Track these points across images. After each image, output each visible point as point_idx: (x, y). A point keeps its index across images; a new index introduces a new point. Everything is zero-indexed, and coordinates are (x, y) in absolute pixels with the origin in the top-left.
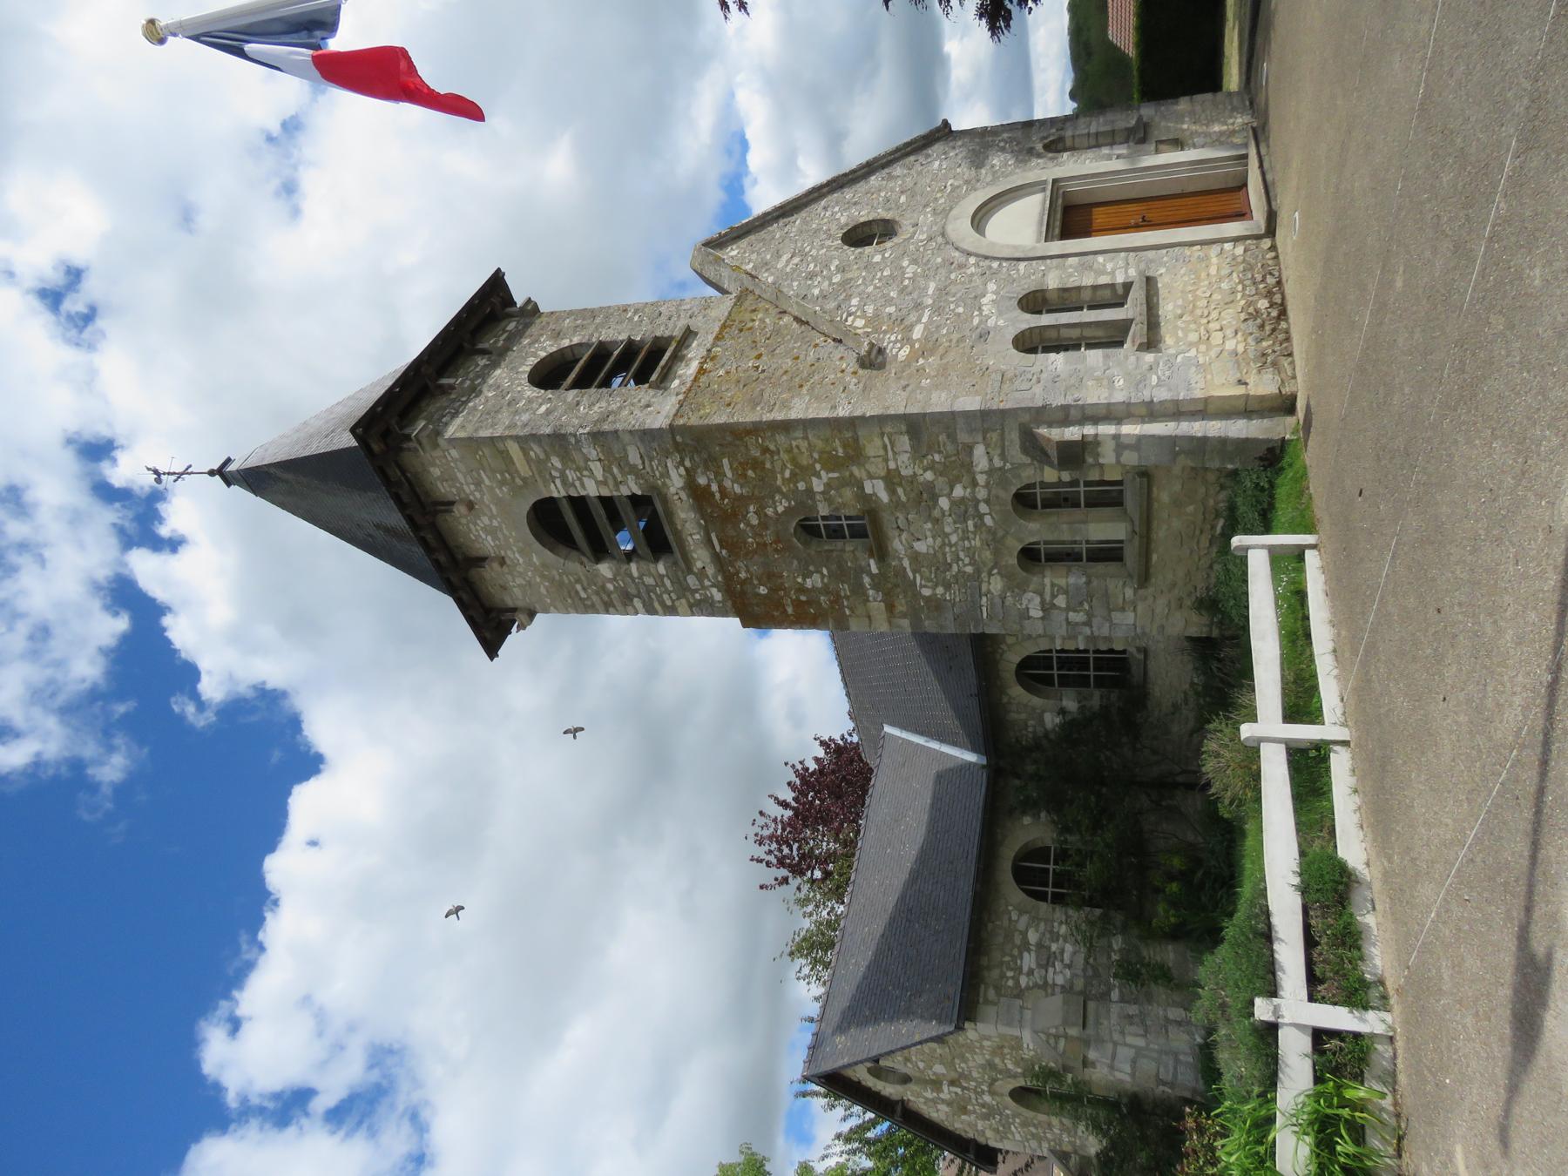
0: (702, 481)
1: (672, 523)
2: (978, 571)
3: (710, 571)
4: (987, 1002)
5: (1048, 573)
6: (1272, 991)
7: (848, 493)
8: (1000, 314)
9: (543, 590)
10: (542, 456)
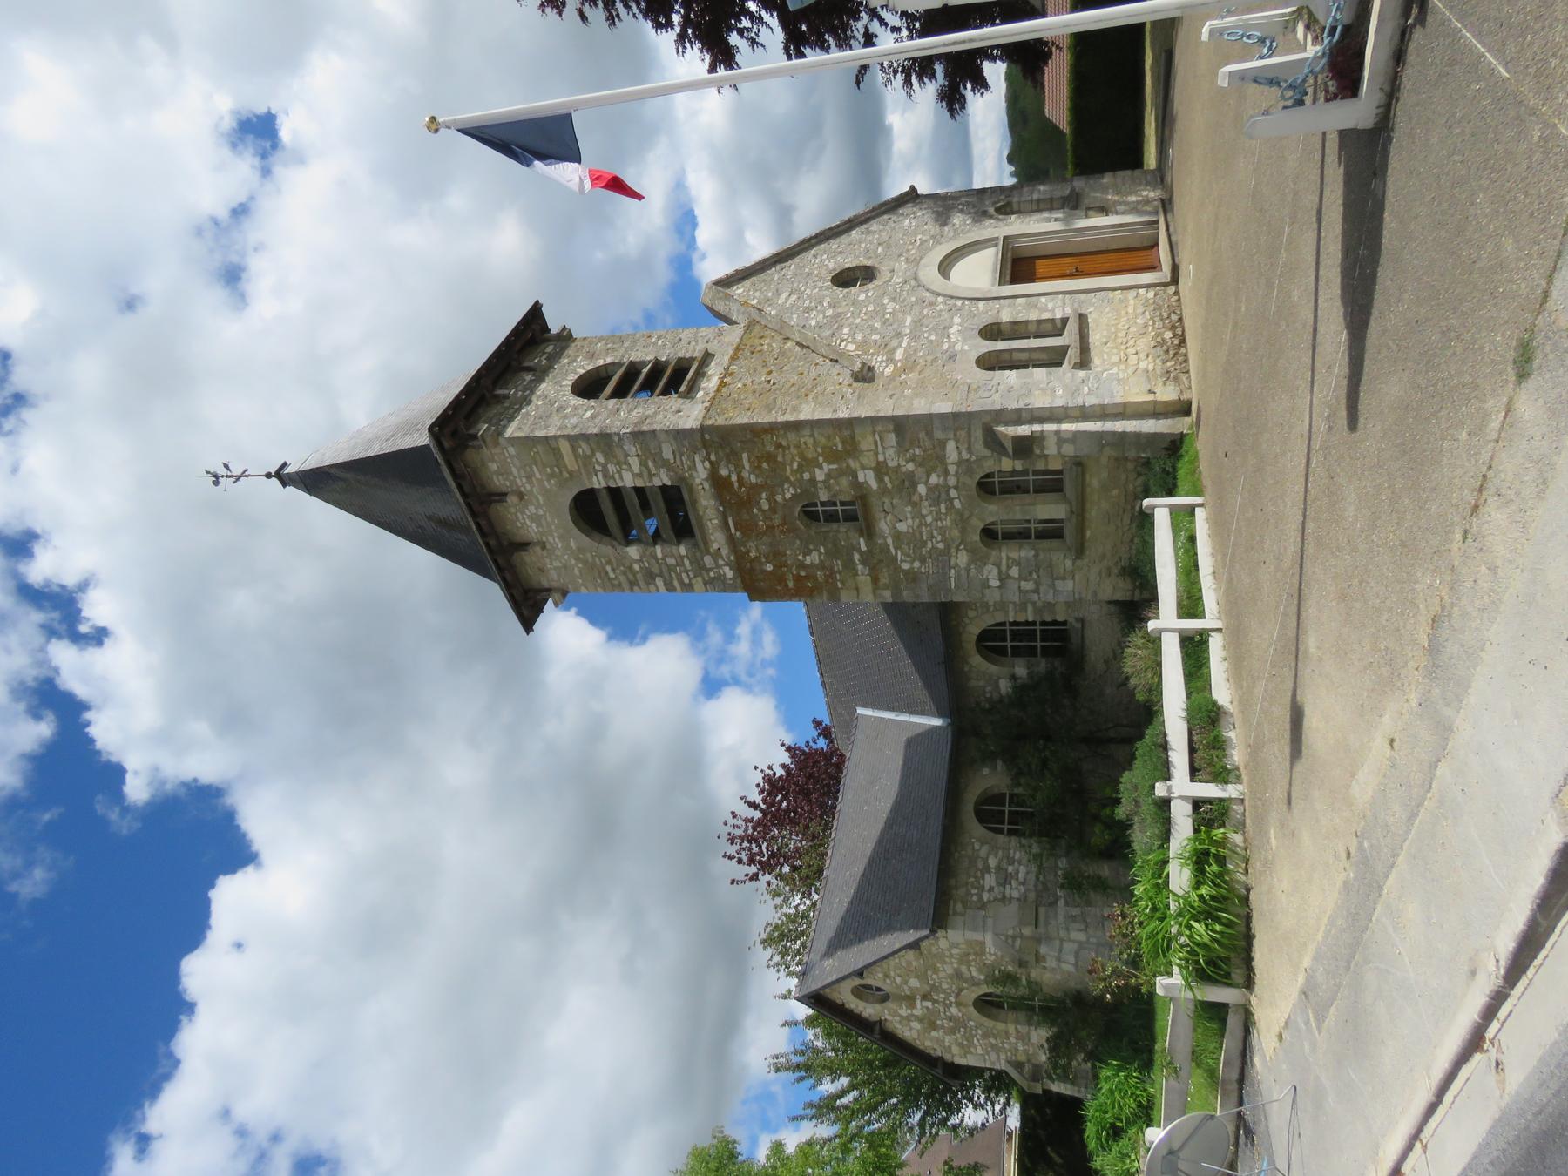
0: (724, 472)
1: (695, 509)
2: (948, 547)
3: (725, 551)
4: (955, 913)
5: (1004, 548)
6: (1167, 777)
7: (845, 482)
8: (965, 341)
9: (576, 572)
10: (589, 452)
